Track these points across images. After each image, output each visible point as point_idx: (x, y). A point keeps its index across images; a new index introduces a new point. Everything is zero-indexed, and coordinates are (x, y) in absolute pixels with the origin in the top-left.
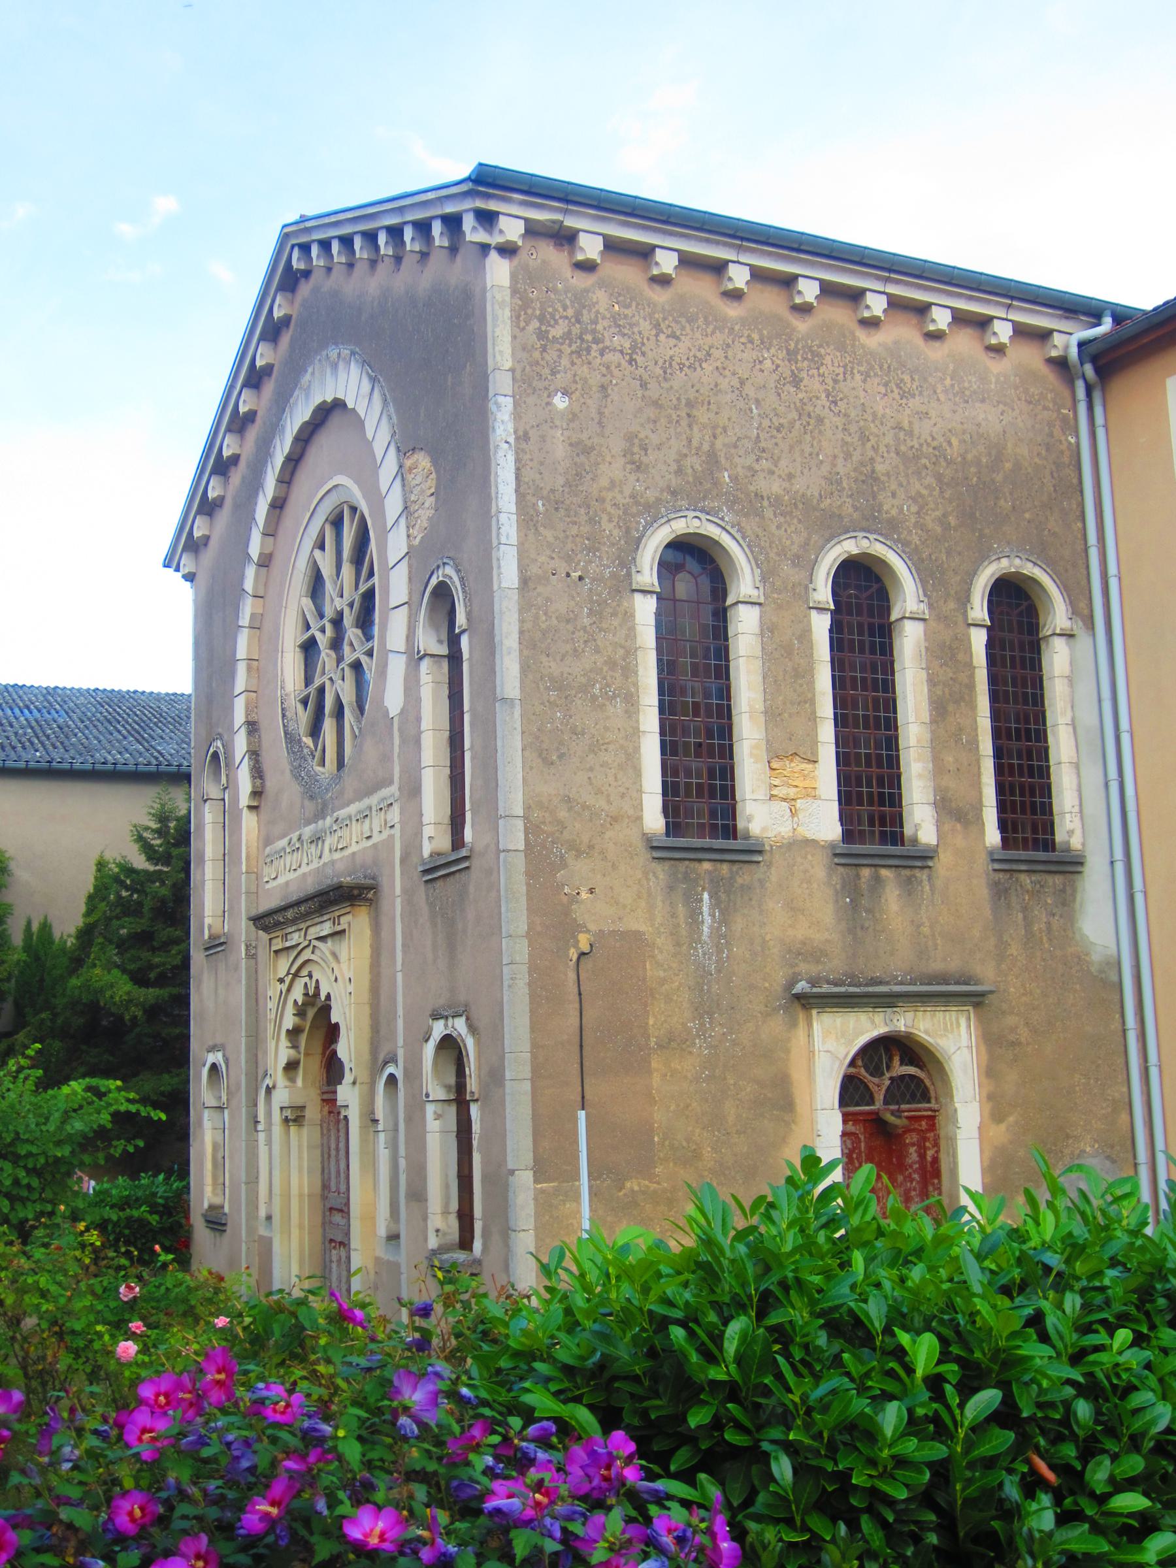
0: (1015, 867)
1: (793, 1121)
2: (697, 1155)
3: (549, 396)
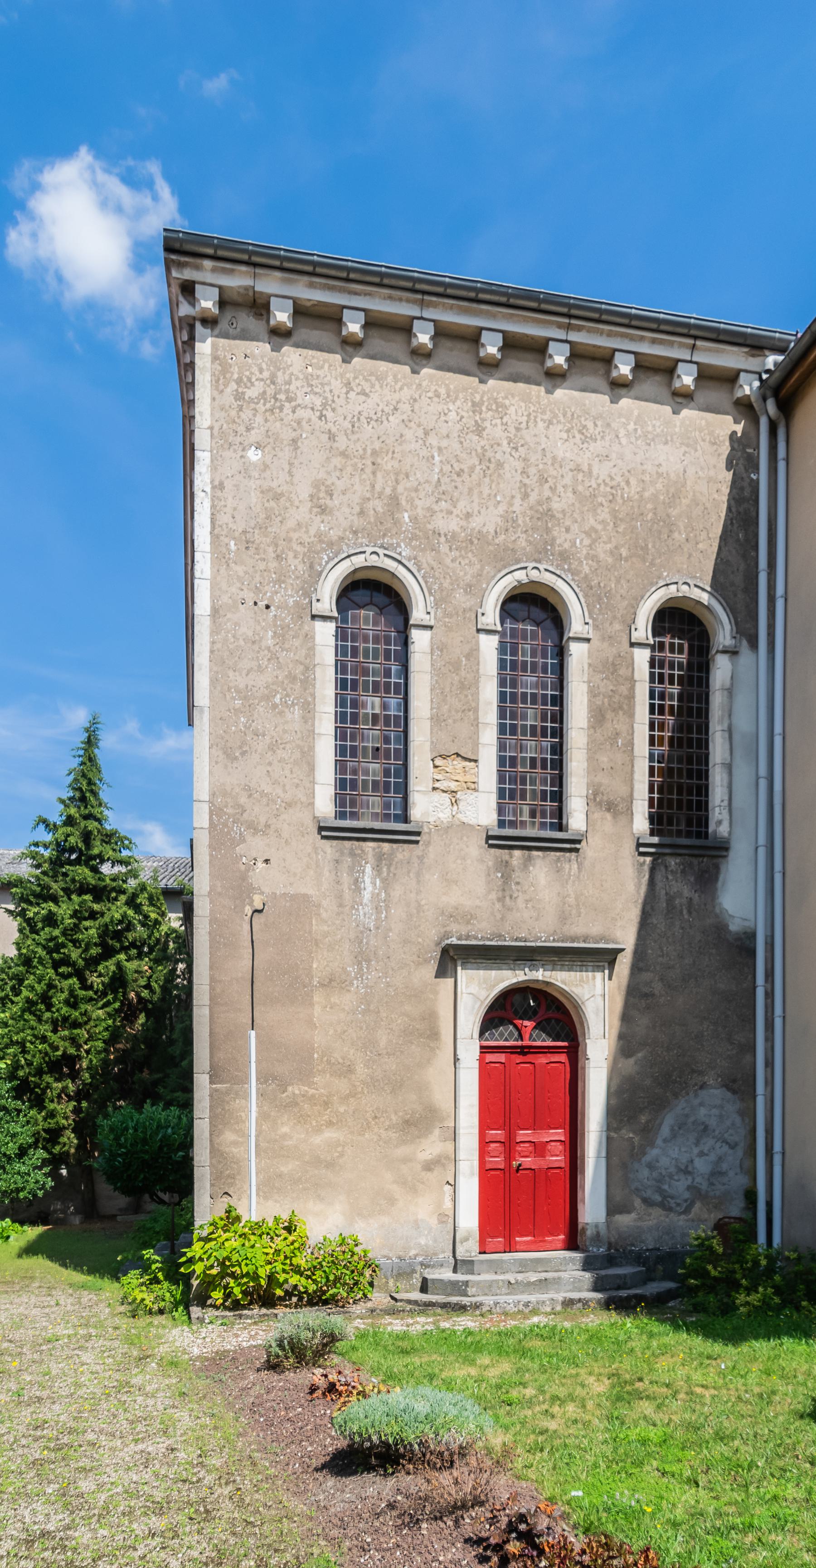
3: (243, 450)
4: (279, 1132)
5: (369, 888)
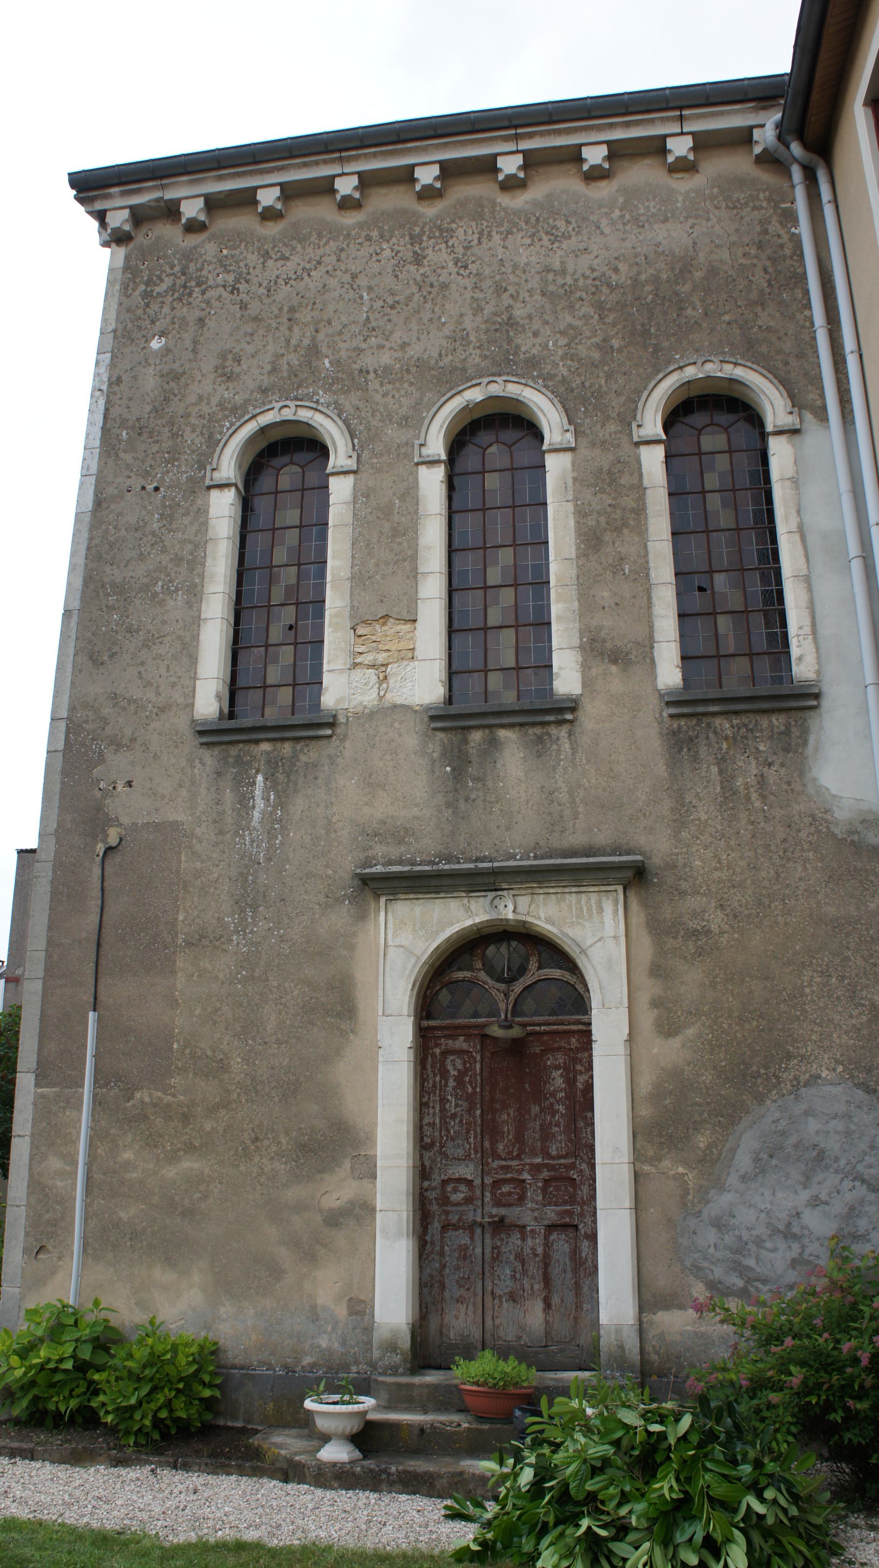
0: (700, 709)
1: (352, 1031)
2: (223, 1067)
3: (146, 342)
4: (119, 1159)
5: (260, 803)
